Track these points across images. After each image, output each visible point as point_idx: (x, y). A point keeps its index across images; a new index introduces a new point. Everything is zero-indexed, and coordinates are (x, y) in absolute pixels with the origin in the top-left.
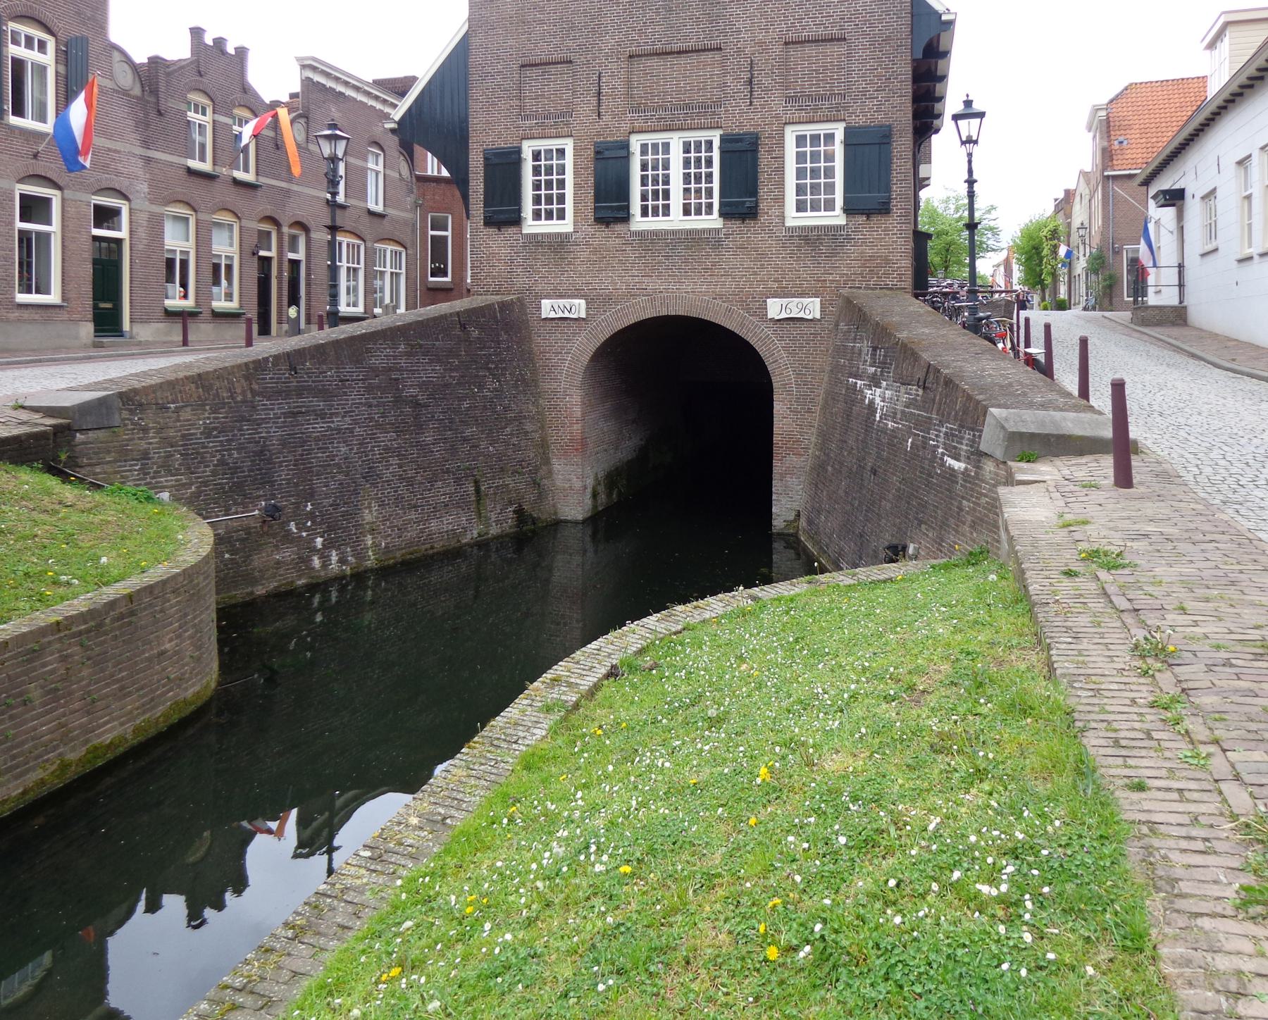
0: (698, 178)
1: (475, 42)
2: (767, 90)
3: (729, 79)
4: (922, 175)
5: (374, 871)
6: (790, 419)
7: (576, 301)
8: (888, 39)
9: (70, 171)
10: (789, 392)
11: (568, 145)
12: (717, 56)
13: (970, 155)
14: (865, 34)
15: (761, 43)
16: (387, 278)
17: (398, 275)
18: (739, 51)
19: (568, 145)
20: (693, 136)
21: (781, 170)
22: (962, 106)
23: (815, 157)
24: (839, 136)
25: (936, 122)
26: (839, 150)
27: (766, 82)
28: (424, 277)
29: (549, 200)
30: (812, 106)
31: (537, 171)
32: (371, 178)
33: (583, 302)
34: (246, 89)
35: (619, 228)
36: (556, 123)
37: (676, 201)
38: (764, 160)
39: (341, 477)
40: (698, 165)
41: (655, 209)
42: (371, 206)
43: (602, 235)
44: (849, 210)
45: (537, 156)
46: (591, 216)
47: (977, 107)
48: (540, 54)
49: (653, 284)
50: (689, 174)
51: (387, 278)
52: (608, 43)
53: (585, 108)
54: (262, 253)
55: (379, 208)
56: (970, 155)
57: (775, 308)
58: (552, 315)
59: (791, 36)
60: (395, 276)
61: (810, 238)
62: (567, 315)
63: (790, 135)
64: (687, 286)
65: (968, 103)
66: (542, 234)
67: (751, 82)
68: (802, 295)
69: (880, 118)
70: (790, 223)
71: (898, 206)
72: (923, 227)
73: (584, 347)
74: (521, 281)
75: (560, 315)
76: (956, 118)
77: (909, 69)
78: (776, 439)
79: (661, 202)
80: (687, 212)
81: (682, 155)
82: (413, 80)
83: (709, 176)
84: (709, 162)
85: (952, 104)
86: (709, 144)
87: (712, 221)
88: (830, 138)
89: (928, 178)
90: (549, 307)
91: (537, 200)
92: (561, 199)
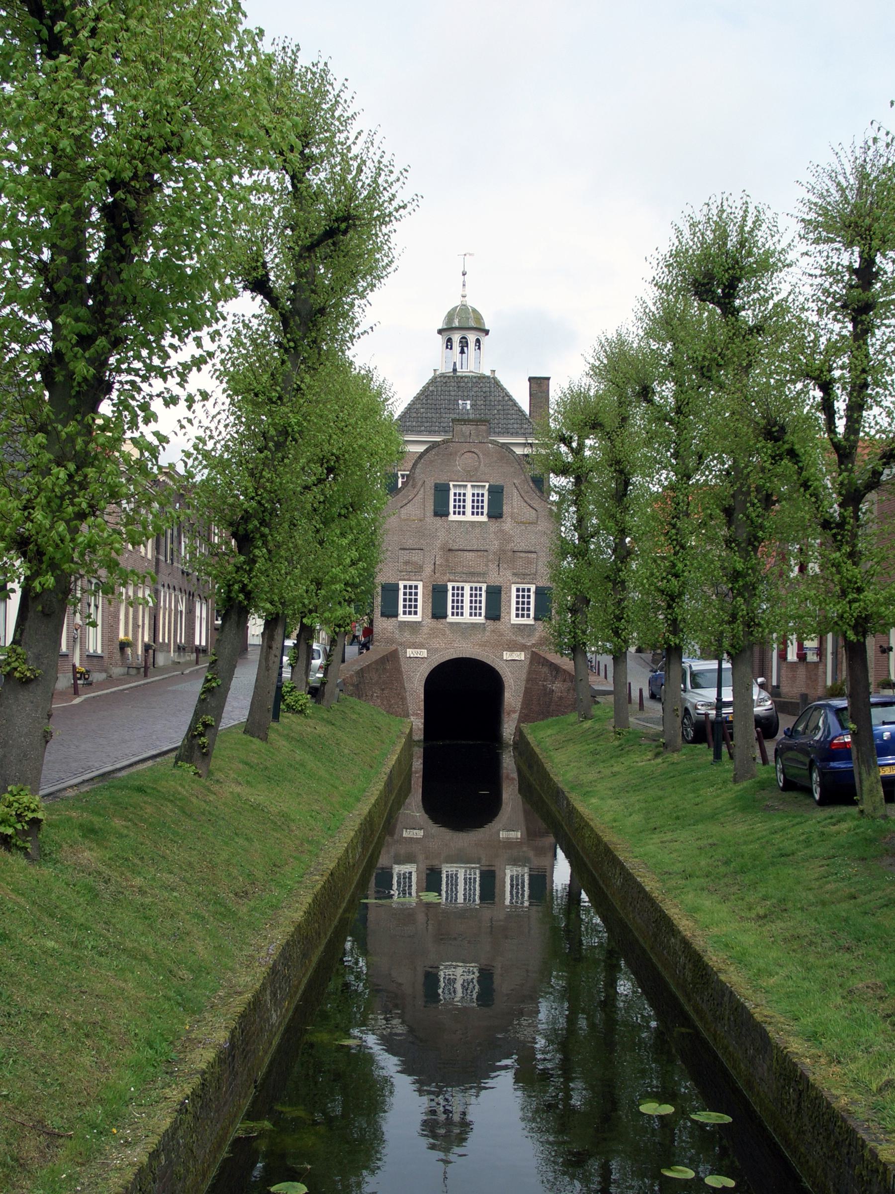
9: (436, 514)
11: (420, 585)
35: (443, 621)
52: (438, 543)
63: (514, 588)
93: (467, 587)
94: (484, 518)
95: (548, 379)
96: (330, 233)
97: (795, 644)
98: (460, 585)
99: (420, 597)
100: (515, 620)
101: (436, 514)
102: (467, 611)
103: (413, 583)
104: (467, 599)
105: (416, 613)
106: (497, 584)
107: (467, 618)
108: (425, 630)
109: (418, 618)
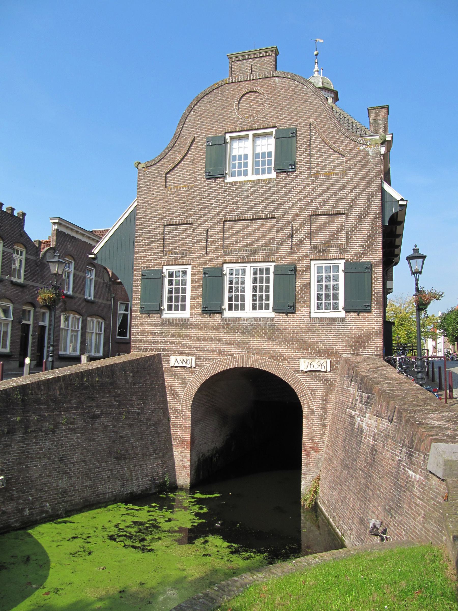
0: (261, 290)
1: (140, 212)
2: (300, 241)
3: (279, 234)
4: (388, 287)
6: (314, 430)
7: (190, 358)
8: (369, 214)
10: (312, 414)
11: (189, 269)
12: (274, 221)
13: (417, 280)
14: (355, 211)
15: (297, 215)
16: (94, 335)
17: (100, 334)
18: (285, 219)
19: (189, 269)
22: (412, 252)
23: (328, 278)
24: (342, 267)
25: (395, 259)
26: (342, 276)
27: (301, 236)
28: (114, 336)
29: (177, 299)
30: (326, 250)
31: (171, 283)
32: (88, 282)
34: (24, 235)
36: (182, 256)
37: (248, 302)
39: (45, 460)
40: (261, 282)
41: (237, 306)
42: (87, 297)
45: (171, 275)
46: (200, 309)
47: (421, 252)
50: (256, 286)
51: (94, 335)
52: (212, 213)
53: (199, 250)
54: (24, 322)
55: (92, 298)
56: (417, 280)
57: (304, 365)
58: (176, 365)
59: (314, 211)
60: (99, 335)
61: (326, 324)
62: (184, 365)
63: (314, 265)
65: (416, 250)
66: (173, 319)
67: (292, 237)
68: (320, 357)
69: (364, 258)
70: (313, 315)
71: (376, 307)
72: (390, 317)
73: (193, 384)
74: (160, 345)
75: (181, 365)
76: (409, 258)
77: (380, 231)
78: (304, 441)
79: (239, 302)
80: (254, 308)
81: (252, 276)
82: (104, 232)
83: (267, 288)
84: (268, 281)
85: (406, 250)
86: (268, 270)
87: (270, 314)
88: (336, 268)
89: (392, 289)
90: (175, 360)
91: (170, 299)
92: (184, 299)
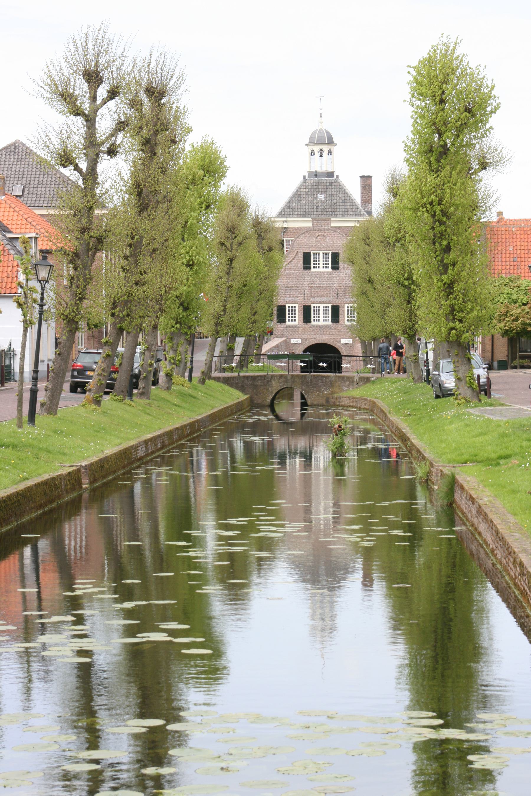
5: (436, 642)
9: (304, 268)
11: (297, 305)
20: (325, 305)
21: (344, 313)
24: (330, 307)
31: (289, 311)
33: (138, 347)
35: (309, 324)
38: (340, 311)
43: (305, 326)
44: (332, 322)
48: (290, 285)
49: (316, 336)
52: (306, 284)
53: (301, 297)
57: (343, 341)
63: (346, 305)
64: (324, 337)
93: (321, 253)
94: (330, 270)
95: (371, 177)
96: (444, 783)
97: (23, 414)
98: (318, 305)
99: (297, 312)
100: (347, 323)
101: (304, 268)
102: (322, 319)
103: (293, 305)
104: (321, 259)
105: (295, 320)
106: (337, 304)
107: (321, 323)
108: (301, 329)
109: (296, 323)
